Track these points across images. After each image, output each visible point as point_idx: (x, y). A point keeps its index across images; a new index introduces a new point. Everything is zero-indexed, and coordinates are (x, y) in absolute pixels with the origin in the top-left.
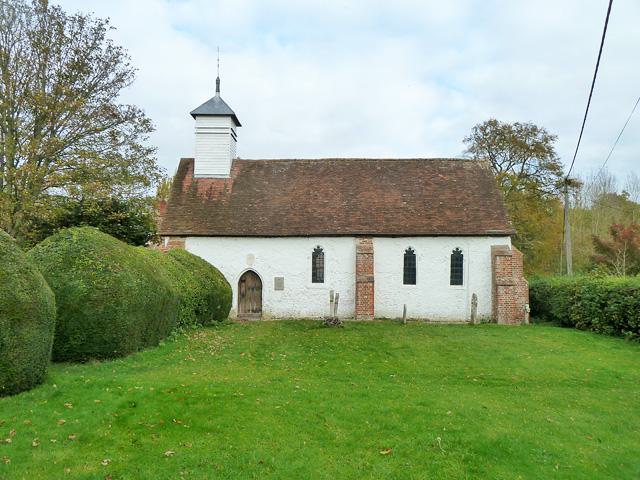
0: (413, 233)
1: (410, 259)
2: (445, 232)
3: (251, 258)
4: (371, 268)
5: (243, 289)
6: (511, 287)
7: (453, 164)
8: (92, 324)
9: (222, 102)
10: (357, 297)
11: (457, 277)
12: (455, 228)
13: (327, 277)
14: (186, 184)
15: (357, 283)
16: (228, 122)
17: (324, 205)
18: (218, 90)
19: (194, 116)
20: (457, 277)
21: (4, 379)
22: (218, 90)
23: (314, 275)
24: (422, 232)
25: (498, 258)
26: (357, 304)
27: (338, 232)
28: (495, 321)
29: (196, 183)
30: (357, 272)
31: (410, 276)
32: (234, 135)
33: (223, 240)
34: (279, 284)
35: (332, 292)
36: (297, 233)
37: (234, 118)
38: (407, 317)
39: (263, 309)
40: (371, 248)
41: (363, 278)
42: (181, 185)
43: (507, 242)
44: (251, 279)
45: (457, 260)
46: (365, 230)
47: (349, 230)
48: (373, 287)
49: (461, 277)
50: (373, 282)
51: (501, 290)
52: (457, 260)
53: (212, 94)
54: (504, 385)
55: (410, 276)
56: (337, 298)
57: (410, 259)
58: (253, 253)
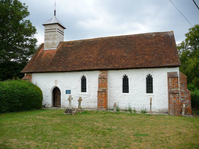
0: (126, 67)
1: (125, 80)
2: (142, 66)
3: (56, 81)
6: (177, 95)
7: (154, 35)
11: (150, 89)
16: (57, 27)
18: (55, 15)
19: (44, 25)
20: (150, 89)
21: (167, 148)
27: (91, 68)
29: (43, 51)
31: (126, 89)
33: (46, 74)
34: (68, 92)
36: (73, 69)
38: (152, 110)
39: (61, 104)
43: (177, 70)
44: (56, 92)
45: (149, 80)
47: (96, 67)
49: (86, 89)
52: (149, 80)
55: (126, 89)
57: (125, 80)
58: (57, 79)
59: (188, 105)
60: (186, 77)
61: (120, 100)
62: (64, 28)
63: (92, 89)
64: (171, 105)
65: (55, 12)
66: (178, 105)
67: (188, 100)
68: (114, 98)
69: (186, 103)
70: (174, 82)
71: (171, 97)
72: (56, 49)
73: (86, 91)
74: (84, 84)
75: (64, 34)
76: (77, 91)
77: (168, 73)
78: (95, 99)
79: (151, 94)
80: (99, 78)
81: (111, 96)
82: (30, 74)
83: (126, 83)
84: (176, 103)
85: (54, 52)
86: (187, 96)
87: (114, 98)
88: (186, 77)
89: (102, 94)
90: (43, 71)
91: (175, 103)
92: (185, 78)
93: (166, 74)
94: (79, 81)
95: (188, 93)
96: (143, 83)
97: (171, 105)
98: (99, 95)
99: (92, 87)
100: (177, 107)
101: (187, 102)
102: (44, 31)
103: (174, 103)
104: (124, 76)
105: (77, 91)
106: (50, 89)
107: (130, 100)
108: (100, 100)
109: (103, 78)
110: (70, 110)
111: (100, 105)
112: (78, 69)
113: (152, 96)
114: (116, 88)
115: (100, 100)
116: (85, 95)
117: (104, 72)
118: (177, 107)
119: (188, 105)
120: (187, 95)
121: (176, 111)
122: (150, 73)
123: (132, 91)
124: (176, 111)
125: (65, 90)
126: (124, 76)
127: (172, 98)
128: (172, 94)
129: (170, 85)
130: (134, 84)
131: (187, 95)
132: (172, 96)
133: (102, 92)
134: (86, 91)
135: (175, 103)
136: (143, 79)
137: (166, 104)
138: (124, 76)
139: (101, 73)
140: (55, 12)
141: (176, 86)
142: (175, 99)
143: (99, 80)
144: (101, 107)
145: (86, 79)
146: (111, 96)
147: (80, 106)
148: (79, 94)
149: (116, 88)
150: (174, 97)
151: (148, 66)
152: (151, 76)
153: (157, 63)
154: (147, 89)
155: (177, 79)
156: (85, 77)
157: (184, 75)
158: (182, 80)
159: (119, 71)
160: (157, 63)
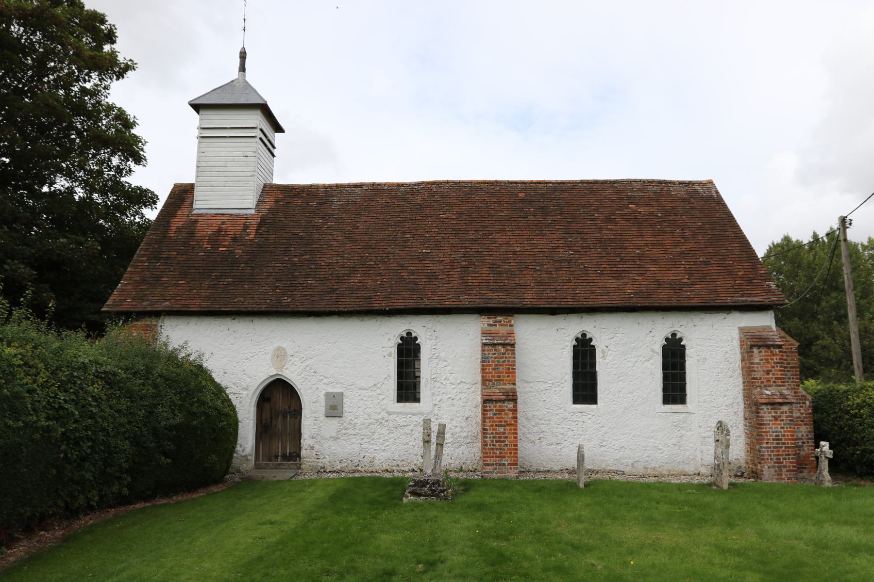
0: (591, 304)
3: (280, 355)
4: (511, 370)
5: (266, 415)
6: (785, 408)
8: (506, 516)
9: (247, 86)
10: (484, 430)
12: (663, 296)
13: (425, 389)
14: (178, 221)
15: (485, 402)
16: (256, 119)
17: (422, 258)
18: (242, 69)
19: (197, 107)
22: (242, 69)
23: (400, 387)
24: (606, 301)
25: (755, 350)
26: (484, 445)
27: (447, 304)
28: (756, 475)
29: (193, 223)
30: (484, 381)
32: (270, 147)
35: (427, 422)
37: (264, 109)
39: (303, 453)
40: (511, 334)
41: (496, 391)
42: (168, 224)
43: (766, 321)
46: (498, 299)
47: (466, 300)
48: (515, 410)
50: (515, 400)
51: (767, 414)
53: (233, 74)
54: (243, 245)
56: (441, 433)
58: (284, 345)
59: (806, 444)
60: (797, 344)
61: (562, 431)
62: (278, 128)
63: (444, 391)
64: (767, 448)
65: (243, 56)
66: (789, 447)
67: (803, 427)
68: (537, 424)
69: (800, 435)
70: (768, 363)
71: (765, 419)
72: (253, 212)
73: (417, 400)
74: (584, 366)
75: (275, 152)
76: (381, 397)
77: (741, 329)
78: (458, 429)
79: (594, 406)
80: (484, 344)
81: (527, 418)
82: (147, 321)
83: (674, 366)
84: (781, 439)
85: (246, 227)
86: (802, 411)
87: (537, 424)
88: (797, 344)
89: (500, 411)
90: (216, 307)
91: (778, 440)
92: (794, 348)
93: (736, 335)
94: (390, 355)
95: (805, 403)
96: (653, 364)
97: (765, 445)
98: (490, 414)
99: (444, 382)
100: (786, 455)
101: (803, 436)
102: (197, 133)
103: (777, 439)
104: (402, 338)
105: (381, 397)
106: (252, 389)
107: (604, 429)
108: (492, 433)
109: (503, 345)
110: (434, 484)
111: (493, 457)
112: (384, 305)
113: (683, 415)
114: (547, 386)
115: (492, 433)
116: (414, 414)
117: (499, 318)
118: (786, 455)
119: (803, 443)
120: (799, 410)
121: (785, 467)
122: (676, 328)
123: (610, 396)
124: (785, 467)
125: (324, 392)
126: (580, 336)
127: (770, 421)
128: (769, 407)
129: (489, 376)
130: (616, 368)
131: (799, 410)
132: (770, 413)
133: (504, 401)
134: (417, 400)
135: (778, 440)
136: (653, 350)
137: (738, 442)
138: (580, 336)
139: (490, 325)
140: (243, 56)
141: (776, 378)
142: (780, 424)
143: (483, 350)
144: (500, 465)
145: (418, 348)
146: (527, 418)
147: (728, 458)
148: (390, 409)
149: (547, 386)
150: (776, 419)
151: (674, 303)
152: (681, 339)
153: (697, 293)
154: (665, 389)
155: (777, 350)
156: (416, 338)
157: (789, 338)
158: (785, 357)
159: (561, 317)
160: (697, 293)
